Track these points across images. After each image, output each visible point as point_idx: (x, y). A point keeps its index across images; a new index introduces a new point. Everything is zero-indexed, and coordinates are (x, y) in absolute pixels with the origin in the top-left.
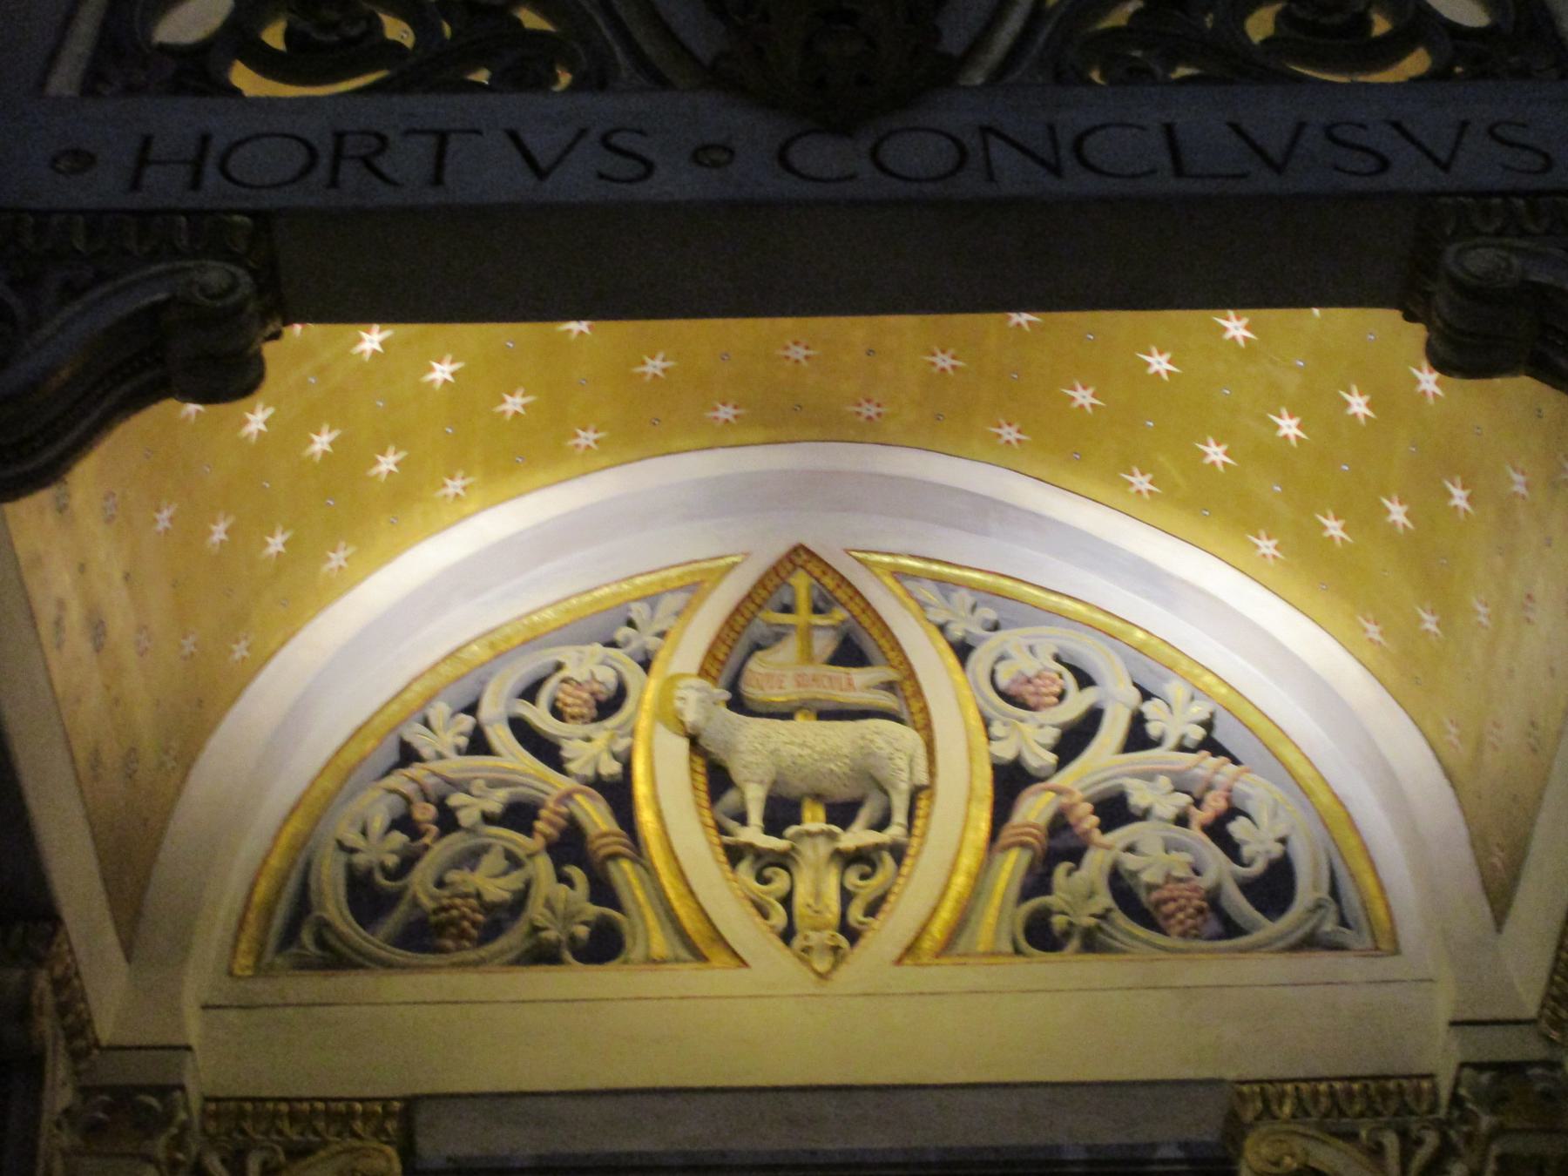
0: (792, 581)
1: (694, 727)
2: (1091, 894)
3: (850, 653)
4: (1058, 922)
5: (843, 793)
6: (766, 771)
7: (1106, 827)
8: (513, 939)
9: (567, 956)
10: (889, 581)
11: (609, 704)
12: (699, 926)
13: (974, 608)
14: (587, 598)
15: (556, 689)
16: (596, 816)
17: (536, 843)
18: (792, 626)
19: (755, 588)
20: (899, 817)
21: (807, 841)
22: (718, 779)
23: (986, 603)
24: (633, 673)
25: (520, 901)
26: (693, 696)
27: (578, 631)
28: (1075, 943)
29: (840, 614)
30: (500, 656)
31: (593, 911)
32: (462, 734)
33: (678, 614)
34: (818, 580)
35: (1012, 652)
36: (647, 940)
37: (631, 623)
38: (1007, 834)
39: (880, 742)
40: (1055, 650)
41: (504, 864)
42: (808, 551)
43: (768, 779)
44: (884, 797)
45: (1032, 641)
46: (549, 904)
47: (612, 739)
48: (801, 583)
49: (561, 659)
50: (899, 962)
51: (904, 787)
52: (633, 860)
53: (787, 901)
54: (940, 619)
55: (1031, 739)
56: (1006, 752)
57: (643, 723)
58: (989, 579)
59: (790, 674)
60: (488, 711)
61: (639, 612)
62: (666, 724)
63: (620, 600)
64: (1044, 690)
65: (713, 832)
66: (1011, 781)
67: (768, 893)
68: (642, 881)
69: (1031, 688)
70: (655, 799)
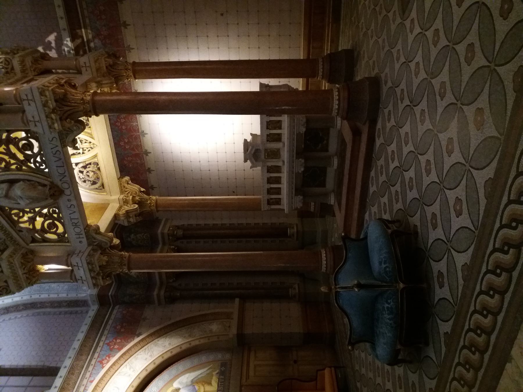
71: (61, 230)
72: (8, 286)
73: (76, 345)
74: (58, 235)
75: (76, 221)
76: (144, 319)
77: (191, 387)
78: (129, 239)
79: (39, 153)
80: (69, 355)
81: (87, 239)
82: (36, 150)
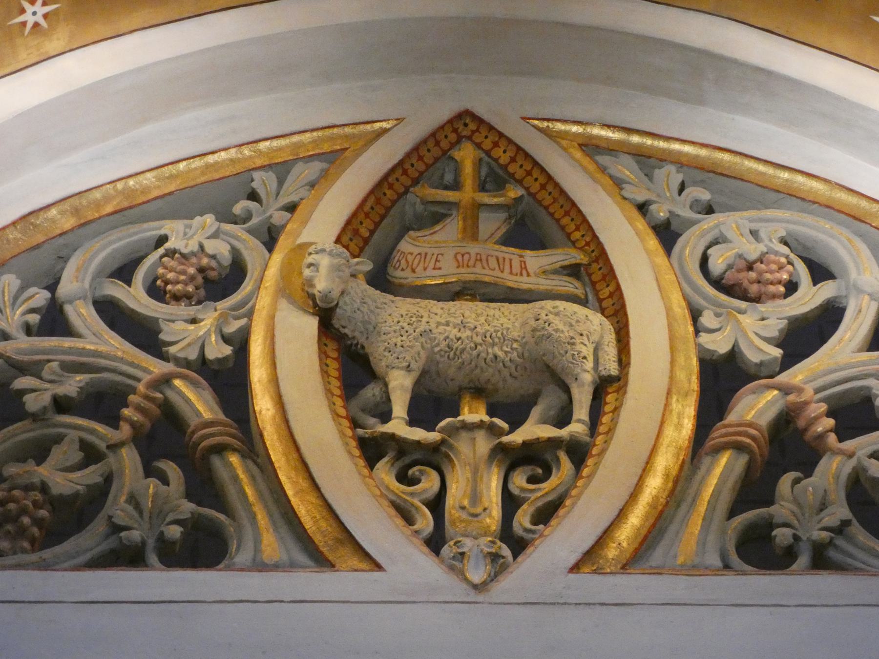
0: (457, 154)
1: (326, 296)
2: (823, 506)
3: (524, 234)
4: (782, 536)
5: (513, 388)
6: (416, 354)
7: (845, 432)
8: (91, 539)
9: (153, 558)
10: (578, 154)
11: (222, 282)
12: (323, 524)
13: (682, 188)
14: (198, 163)
15: (155, 266)
16: (198, 403)
17: (125, 431)
18: (456, 205)
19: (408, 155)
20: (581, 412)
21: (464, 435)
22: (352, 365)
23: (695, 183)
24: (252, 251)
25: (100, 494)
26: (325, 262)
27: (183, 202)
28: (803, 560)
29: (514, 192)
30: (87, 228)
31: (188, 508)
32: (32, 311)
33: (312, 185)
34: (488, 153)
35: (729, 235)
36: (257, 541)
37: (253, 196)
38: (718, 434)
39: (558, 323)
40: (784, 234)
41: (77, 456)
42: (480, 121)
43: (417, 367)
44: (564, 397)
45: (754, 226)
46: (133, 500)
47: (223, 318)
48: (466, 155)
49: (162, 232)
50: (575, 568)
51: (588, 378)
52: (244, 456)
53: (437, 504)
54: (641, 198)
55: (753, 332)
56: (719, 344)
57: (263, 301)
58: (703, 152)
59: (450, 254)
60: (65, 288)
61: (264, 182)
62: (291, 300)
63: (239, 168)
64: (768, 276)
65: (346, 423)
66: (722, 379)
67: (412, 494)
68: (253, 478)
69: (753, 275)
70: (274, 381)
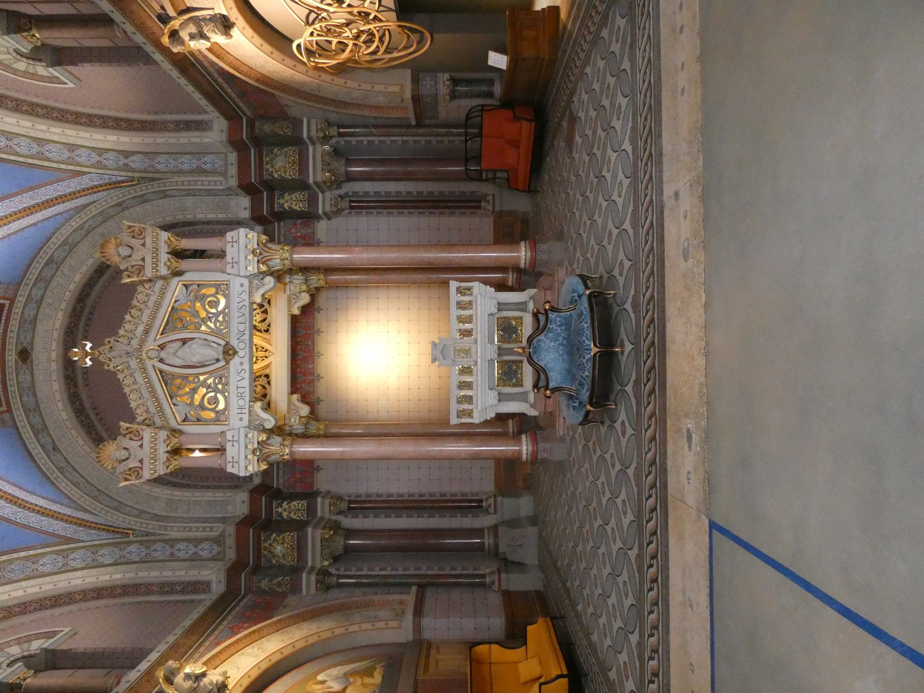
8: (267, 386)
71: (221, 406)
72: (141, 468)
73: (187, 623)
74: (217, 412)
75: (241, 390)
76: (286, 606)
77: (343, 679)
78: (280, 510)
79: (223, 312)
80: (175, 632)
81: (250, 416)
82: (220, 308)
